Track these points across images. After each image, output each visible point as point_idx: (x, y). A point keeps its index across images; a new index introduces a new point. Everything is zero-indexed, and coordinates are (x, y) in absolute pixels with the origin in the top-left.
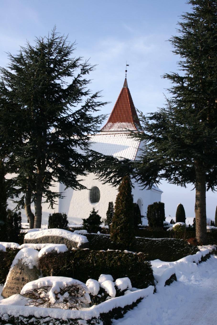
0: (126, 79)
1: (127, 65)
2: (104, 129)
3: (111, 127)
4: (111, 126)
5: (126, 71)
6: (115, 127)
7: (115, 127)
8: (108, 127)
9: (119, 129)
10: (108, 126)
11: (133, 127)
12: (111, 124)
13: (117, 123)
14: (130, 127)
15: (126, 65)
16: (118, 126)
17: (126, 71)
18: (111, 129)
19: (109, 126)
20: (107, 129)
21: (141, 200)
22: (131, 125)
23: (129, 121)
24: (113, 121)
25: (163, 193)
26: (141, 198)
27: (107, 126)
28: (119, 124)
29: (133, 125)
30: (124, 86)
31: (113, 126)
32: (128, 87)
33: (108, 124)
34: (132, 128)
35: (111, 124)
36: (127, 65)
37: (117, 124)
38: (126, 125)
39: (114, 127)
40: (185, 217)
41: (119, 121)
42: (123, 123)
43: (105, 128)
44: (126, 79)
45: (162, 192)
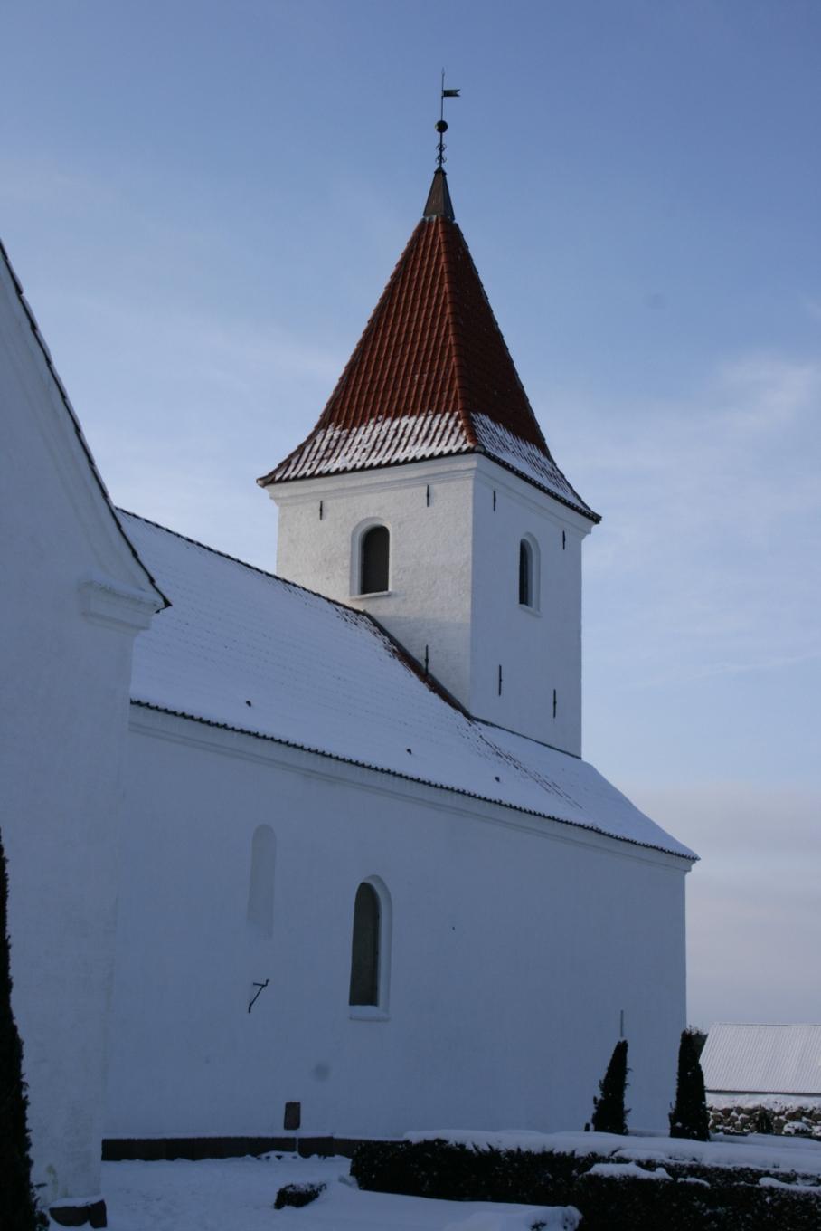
0: (440, 173)
1: (448, 94)
2: (291, 468)
3: (331, 451)
4: (333, 444)
5: (442, 127)
6: (353, 449)
7: (353, 449)
8: (312, 455)
9: (374, 454)
10: (316, 448)
11: (457, 431)
12: (333, 433)
13: (371, 426)
14: (438, 438)
15: (441, 94)
16: (371, 443)
17: (442, 127)
18: (332, 460)
19: (323, 448)
20: (308, 465)
21: (379, 892)
22: (452, 423)
23: (440, 403)
24: (347, 419)
25: (695, 867)
26: (379, 879)
27: (307, 450)
28: (377, 429)
29: (460, 423)
30: (425, 214)
31: (341, 442)
32: (460, 219)
33: (319, 438)
34: (462, 440)
35: (336, 436)
36: (448, 94)
37: (366, 434)
38: (417, 429)
39: (346, 449)
40: (8, 963)
41: (380, 413)
42: (405, 421)
43: (294, 461)
44: (440, 173)
45: (695, 859)
